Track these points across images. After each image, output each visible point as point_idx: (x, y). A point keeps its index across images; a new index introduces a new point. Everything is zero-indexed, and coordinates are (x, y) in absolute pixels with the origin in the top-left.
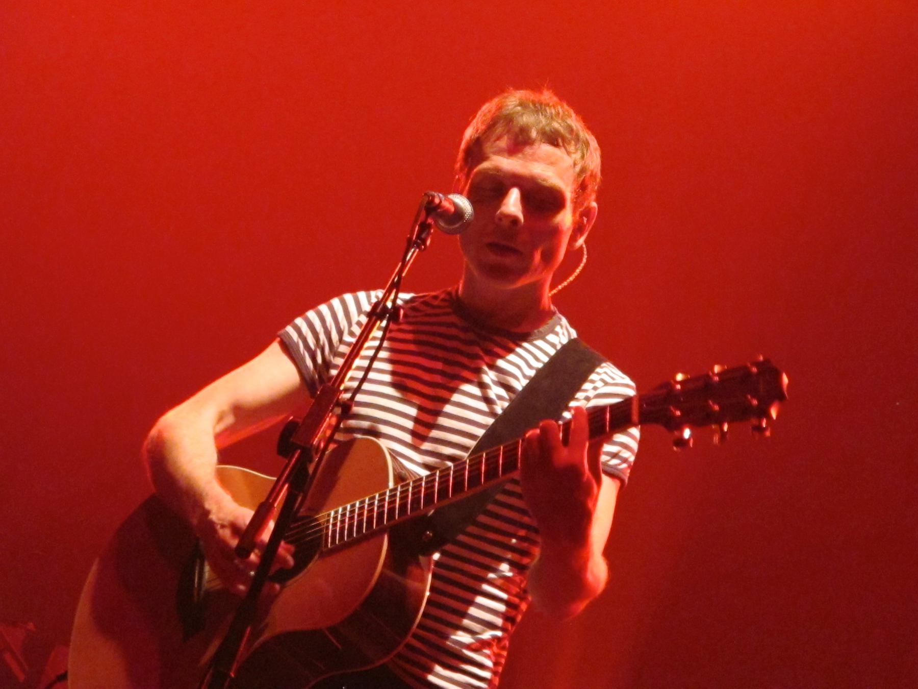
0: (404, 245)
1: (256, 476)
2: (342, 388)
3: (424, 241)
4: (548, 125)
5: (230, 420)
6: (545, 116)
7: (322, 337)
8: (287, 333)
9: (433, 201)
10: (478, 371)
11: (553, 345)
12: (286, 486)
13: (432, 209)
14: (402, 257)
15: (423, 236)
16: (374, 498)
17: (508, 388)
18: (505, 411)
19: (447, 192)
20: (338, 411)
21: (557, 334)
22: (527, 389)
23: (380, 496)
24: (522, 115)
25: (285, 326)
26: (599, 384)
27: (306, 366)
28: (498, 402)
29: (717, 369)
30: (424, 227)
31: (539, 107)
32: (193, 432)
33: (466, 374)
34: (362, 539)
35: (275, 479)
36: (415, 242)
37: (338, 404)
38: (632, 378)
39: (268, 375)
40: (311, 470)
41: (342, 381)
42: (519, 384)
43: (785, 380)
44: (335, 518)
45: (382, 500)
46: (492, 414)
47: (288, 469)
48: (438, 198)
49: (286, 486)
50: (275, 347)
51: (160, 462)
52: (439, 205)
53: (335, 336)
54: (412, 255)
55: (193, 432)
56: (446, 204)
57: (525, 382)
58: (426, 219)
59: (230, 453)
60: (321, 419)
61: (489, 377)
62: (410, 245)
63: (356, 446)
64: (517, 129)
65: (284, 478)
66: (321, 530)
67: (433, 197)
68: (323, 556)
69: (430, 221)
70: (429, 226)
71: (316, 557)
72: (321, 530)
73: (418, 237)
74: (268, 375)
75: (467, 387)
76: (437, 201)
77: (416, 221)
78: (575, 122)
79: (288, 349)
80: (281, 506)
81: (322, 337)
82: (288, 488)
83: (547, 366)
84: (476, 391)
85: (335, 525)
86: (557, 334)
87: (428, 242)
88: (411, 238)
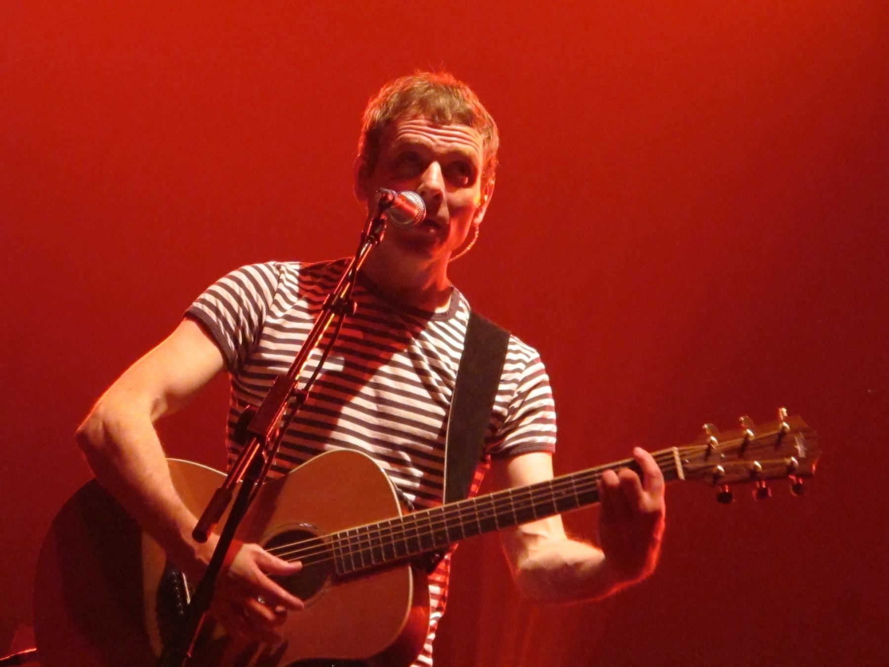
0: (359, 240)
2: (297, 378)
4: (462, 107)
5: (163, 408)
6: (458, 97)
9: (386, 198)
10: (408, 343)
11: (462, 322)
13: (385, 204)
15: (377, 231)
19: (398, 190)
20: (293, 399)
21: (461, 310)
24: (438, 98)
25: (191, 303)
30: (378, 222)
31: (449, 90)
33: (397, 345)
36: (369, 238)
37: (294, 393)
41: (298, 372)
47: (249, 462)
48: (391, 194)
52: (392, 202)
53: (254, 317)
54: (366, 249)
56: (399, 201)
58: (380, 216)
60: (277, 409)
61: (417, 347)
62: (363, 240)
64: (433, 109)
67: (387, 194)
69: (383, 217)
70: (383, 222)
74: (187, 358)
75: (397, 357)
76: (390, 198)
77: (369, 219)
78: (472, 103)
84: (407, 362)
87: (382, 238)
88: (365, 234)
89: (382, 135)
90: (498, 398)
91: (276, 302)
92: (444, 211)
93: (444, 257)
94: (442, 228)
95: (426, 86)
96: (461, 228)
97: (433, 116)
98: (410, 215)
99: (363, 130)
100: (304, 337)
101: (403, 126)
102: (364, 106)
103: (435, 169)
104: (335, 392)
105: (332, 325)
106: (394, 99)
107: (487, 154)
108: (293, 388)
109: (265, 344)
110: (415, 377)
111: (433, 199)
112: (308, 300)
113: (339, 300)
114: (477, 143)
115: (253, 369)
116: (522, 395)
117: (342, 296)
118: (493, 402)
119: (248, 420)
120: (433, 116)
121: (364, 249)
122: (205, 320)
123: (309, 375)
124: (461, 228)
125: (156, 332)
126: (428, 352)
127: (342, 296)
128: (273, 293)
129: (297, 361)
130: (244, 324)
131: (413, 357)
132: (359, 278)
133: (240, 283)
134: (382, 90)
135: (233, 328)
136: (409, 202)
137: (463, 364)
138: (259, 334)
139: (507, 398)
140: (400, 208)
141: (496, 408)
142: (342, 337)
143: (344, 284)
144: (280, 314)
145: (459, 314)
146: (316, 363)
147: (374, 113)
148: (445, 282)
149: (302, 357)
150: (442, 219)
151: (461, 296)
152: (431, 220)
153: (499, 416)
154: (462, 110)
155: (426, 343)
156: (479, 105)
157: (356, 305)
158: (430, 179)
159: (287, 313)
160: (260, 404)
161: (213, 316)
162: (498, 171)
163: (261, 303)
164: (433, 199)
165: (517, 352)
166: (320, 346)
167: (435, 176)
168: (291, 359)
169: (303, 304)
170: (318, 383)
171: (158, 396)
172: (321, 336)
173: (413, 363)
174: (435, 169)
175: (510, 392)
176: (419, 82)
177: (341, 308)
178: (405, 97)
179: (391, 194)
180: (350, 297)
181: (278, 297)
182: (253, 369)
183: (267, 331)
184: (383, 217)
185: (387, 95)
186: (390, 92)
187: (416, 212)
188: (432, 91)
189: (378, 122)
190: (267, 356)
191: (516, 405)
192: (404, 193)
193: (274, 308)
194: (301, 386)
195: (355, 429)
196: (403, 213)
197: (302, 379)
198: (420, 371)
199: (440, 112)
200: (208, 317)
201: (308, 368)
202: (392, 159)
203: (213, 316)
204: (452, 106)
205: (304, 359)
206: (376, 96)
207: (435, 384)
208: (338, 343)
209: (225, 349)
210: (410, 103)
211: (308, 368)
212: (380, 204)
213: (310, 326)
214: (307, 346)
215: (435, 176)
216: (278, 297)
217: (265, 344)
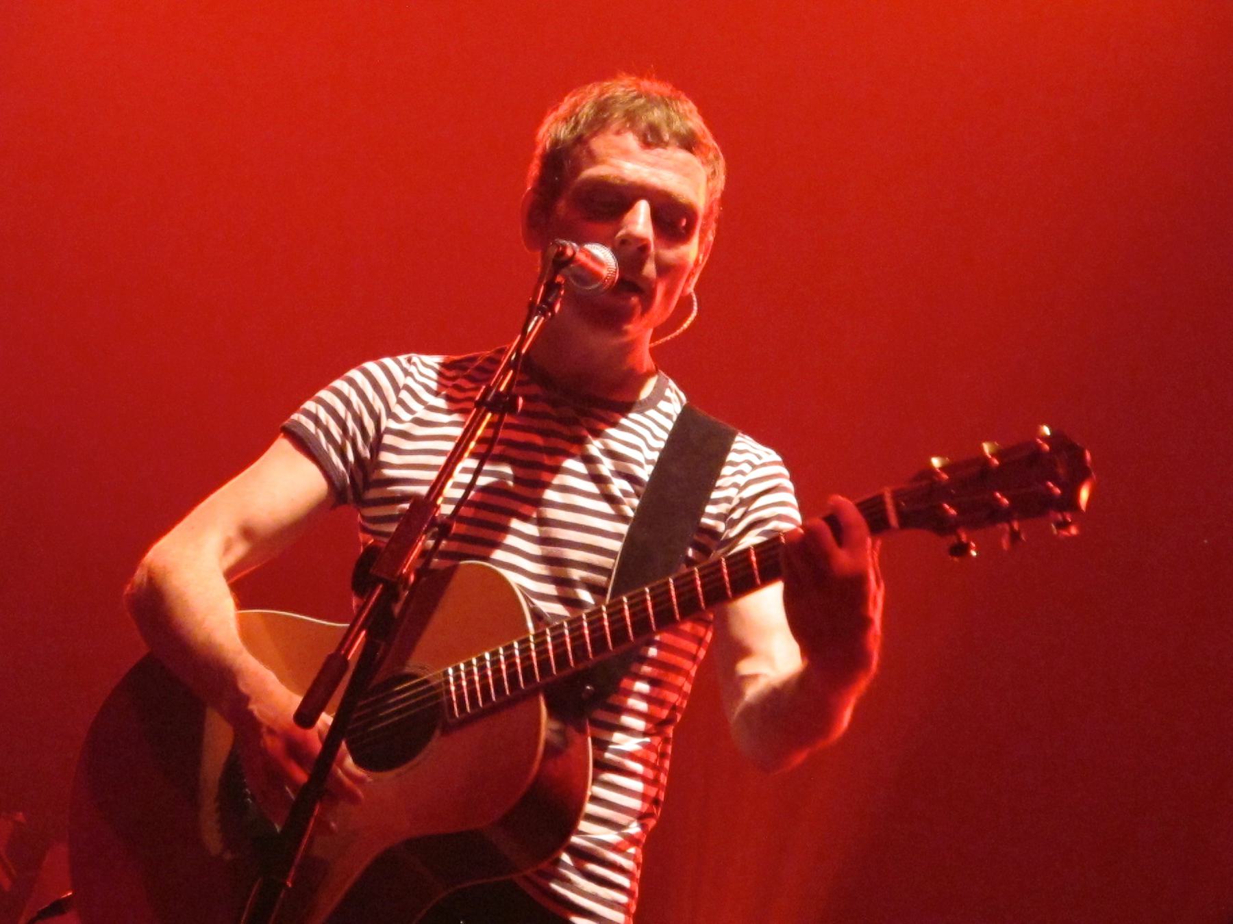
0: (525, 312)
1: (279, 616)
3: (551, 307)
7: (351, 424)
8: (299, 424)
9: (563, 253)
11: (668, 416)
12: (363, 633)
13: (561, 262)
14: (521, 326)
16: (511, 647)
17: (632, 479)
18: (639, 511)
19: (581, 241)
21: (668, 400)
22: (653, 476)
23: (520, 643)
26: (746, 467)
27: (335, 468)
28: (625, 500)
29: (987, 448)
30: (552, 287)
31: (665, 102)
32: (196, 564)
34: (507, 704)
35: (347, 625)
36: (540, 308)
37: (434, 522)
38: (779, 452)
39: (282, 484)
40: (397, 609)
42: (645, 473)
43: (1088, 456)
44: (458, 678)
45: (525, 651)
46: (622, 518)
48: (571, 248)
49: (363, 633)
50: (283, 445)
51: (155, 609)
52: (572, 259)
55: (196, 564)
56: (581, 257)
57: (650, 469)
59: (249, 586)
60: (412, 544)
62: (532, 310)
63: (458, 576)
65: (360, 623)
66: (437, 696)
67: (565, 247)
68: (447, 730)
69: (559, 279)
70: (559, 286)
71: (437, 733)
72: (437, 696)
73: (544, 300)
74: (282, 484)
75: (570, 463)
76: (569, 252)
78: (695, 123)
79: (304, 445)
80: (357, 658)
81: (351, 424)
82: (366, 636)
83: (669, 443)
85: (459, 687)
86: (668, 400)
89: (562, 162)
90: (710, 509)
91: (401, 402)
92: (650, 269)
93: (642, 335)
94: (647, 295)
95: (632, 94)
96: (669, 294)
97: (645, 136)
98: (596, 276)
99: (539, 151)
100: (449, 446)
101: (598, 144)
102: (539, 122)
103: (643, 209)
104: (487, 517)
105: (489, 425)
106: (587, 111)
107: (710, 193)
108: (434, 518)
109: (385, 457)
110: (592, 487)
111: (632, 254)
112: (449, 398)
113: (498, 394)
114: (692, 179)
115: (373, 494)
116: (744, 502)
117: (502, 389)
118: (702, 513)
119: (372, 567)
120: (645, 136)
121: (533, 324)
122: (300, 433)
123: (458, 494)
124: (669, 294)
125: (241, 455)
126: (611, 454)
127: (502, 389)
128: (397, 390)
129: (439, 477)
130: (354, 434)
131: (589, 460)
132: (524, 365)
133: (316, 419)
134: (566, 99)
135: (339, 439)
136: (594, 259)
137: (661, 466)
138: (377, 446)
139: (723, 508)
140: (583, 266)
141: (705, 521)
142: (502, 442)
143: (504, 373)
144: (406, 416)
145: (662, 405)
146: (467, 478)
147: (553, 130)
148: (648, 362)
149: (446, 472)
150: (646, 279)
151: (672, 383)
152: (631, 283)
153: (712, 533)
154: (683, 131)
155: (602, 447)
156: (703, 126)
157: (521, 401)
158: (635, 222)
159: (417, 415)
160: (386, 540)
161: (311, 426)
162: (718, 221)
163: (378, 405)
164: (632, 254)
165: (741, 452)
166: (473, 455)
167: (640, 221)
168: (432, 475)
169: (441, 403)
170: (472, 504)
171: (232, 532)
172: (472, 445)
173: (589, 469)
174: (643, 209)
175: (728, 500)
176: (621, 89)
177: (502, 404)
178: (603, 107)
179: (571, 248)
180: (514, 389)
181: (404, 395)
182: (373, 494)
183: (388, 439)
184: (559, 279)
185: (575, 105)
186: (584, 102)
187: (605, 272)
188: (642, 101)
189: (564, 141)
190: (389, 473)
191: (736, 515)
192: (588, 247)
193: (398, 410)
194: (447, 509)
195: (517, 560)
196: (588, 275)
197: (448, 501)
198: (598, 479)
199: (654, 129)
200: (306, 430)
201: (457, 485)
202: (575, 199)
203: (311, 426)
204: (669, 122)
205: (450, 475)
206: (556, 109)
207: (618, 494)
208: (497, 449)
209: (329, 468)
210: (612, 115)
211: (457, 485)
212: (554, 262)
213: (458, 432)
214: (454, 458)
215: (640, 221)
216: (404, 395)
217: (385, 457)
